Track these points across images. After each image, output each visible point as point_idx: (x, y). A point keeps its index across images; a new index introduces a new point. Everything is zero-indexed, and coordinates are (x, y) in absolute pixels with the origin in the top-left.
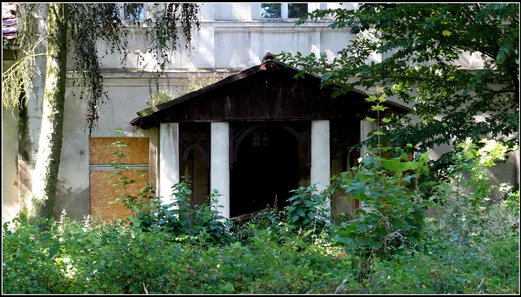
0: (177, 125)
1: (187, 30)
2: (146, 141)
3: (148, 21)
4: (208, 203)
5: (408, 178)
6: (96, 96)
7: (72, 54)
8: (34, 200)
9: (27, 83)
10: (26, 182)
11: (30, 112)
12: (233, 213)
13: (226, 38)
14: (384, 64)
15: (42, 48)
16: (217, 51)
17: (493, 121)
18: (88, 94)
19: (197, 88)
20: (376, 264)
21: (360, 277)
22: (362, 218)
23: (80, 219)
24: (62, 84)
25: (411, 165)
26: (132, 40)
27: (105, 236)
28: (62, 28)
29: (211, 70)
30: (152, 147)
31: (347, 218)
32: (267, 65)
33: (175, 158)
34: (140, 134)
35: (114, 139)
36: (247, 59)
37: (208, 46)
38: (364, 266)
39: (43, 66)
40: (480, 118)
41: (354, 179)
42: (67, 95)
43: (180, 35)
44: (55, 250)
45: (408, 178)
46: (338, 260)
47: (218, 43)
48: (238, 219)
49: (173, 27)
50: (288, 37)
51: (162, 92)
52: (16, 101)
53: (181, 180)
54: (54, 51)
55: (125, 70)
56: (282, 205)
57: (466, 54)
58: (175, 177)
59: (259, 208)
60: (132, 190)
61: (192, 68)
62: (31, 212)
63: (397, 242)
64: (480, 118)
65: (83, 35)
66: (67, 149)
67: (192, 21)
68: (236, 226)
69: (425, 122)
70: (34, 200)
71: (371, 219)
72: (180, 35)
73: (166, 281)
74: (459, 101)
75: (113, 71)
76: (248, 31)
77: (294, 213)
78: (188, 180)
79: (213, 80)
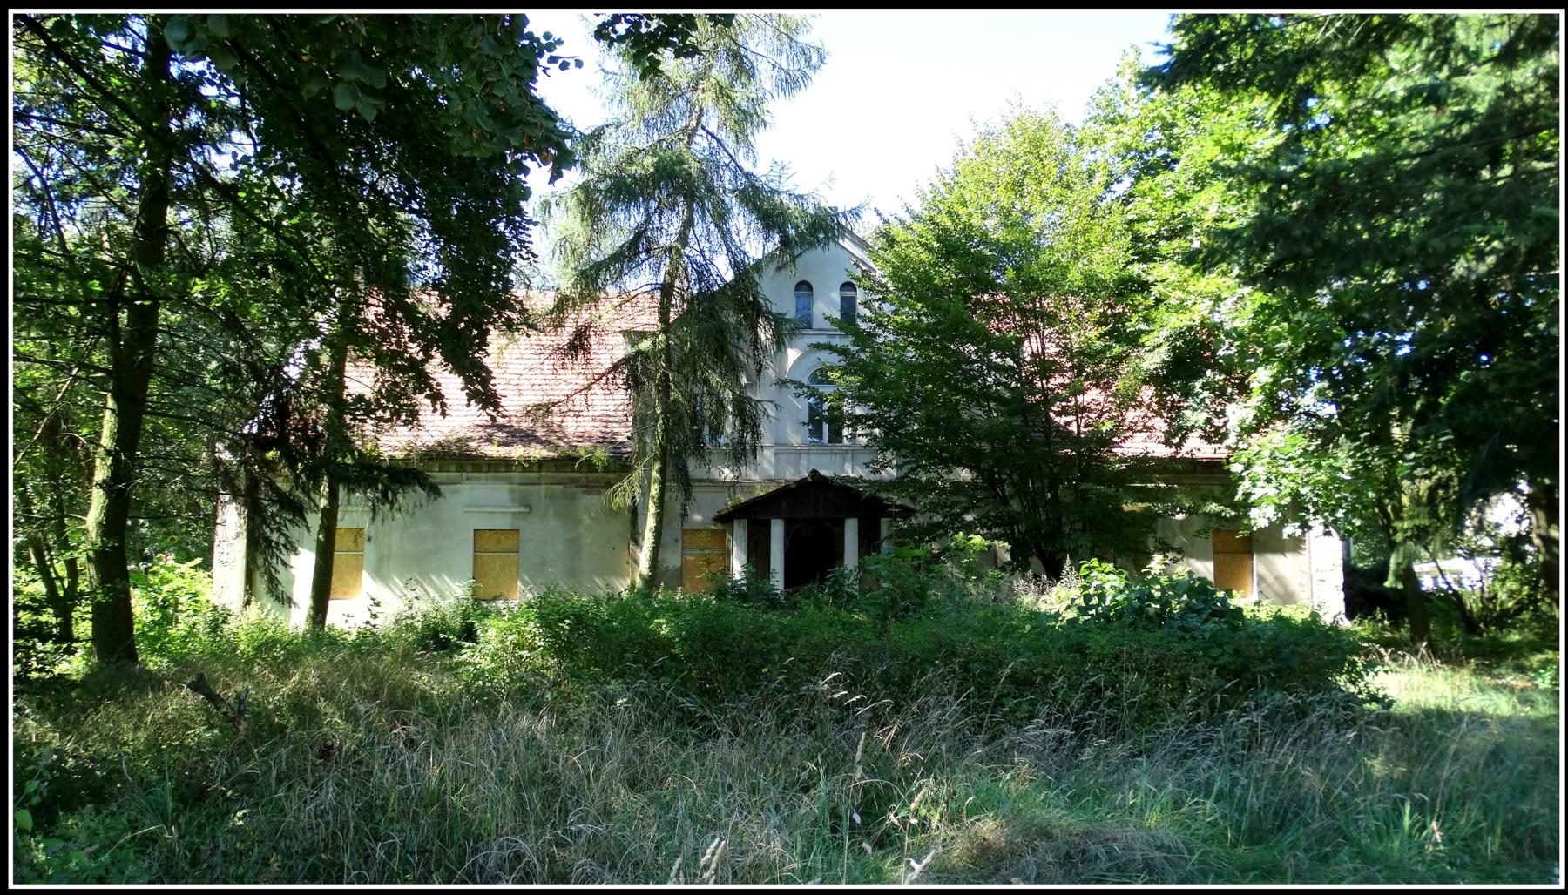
0: (746, 521)
1: (754, 452)
2: (724, 532)
3: (727, 445)
4: (769, 579)
5: (916, 563)
6: (687, 499)
7: (670, 470)
8: (641, 575)
9: (637, 489)
10: (636, 562)
11: (640, 511)
12: (786, 586)
13: (783, 457)
14: (900, 479)
15: (649, 465)
16: (776, 466)
17: (980, 520)
18: (681, 498)
19: (761, 494)
20: (893, 627)
21: (880, 636)
22: (881, 591)
23: (675, 590)
24: (662, 491)
25: (917, 552)
26: (714, 458)
27: (692, 602)
28: (663, 449)
29: (772, 481)
30: (728, 536)
31: (870, 590)
32: (812, 477)
33: (744, 544)
34: (719, 527)
35: (700, 531)
36: (799, 473)
37: (769, 462)
38: (883, 627)
39: (649, 477)
40: (969, 518)
41: (1318, 466)
42: (666, 498)
43: (749, 455)
44: (655, 613)
45: (916, 563)
46: (862, 622)
47: (777, 461)
48: (790, 590)
49: (744, 449)
50: (828, 457)
51: (738, 496)
52: (629, 502)
53: (749, 561)
54: (657, 466)
55: (709, 480)
56: (822, 580)
57: (958, 470)
58: (744, 558)
59: (806, 583)
60: (713, 568)
61: (756, 478)
62: (639, 583)
63: (906, 609)
64: (969, 518)
65: (678, 455)
66: (665, 537)
67: (758, 445)
68: (788, 595)
69: (1156, 563)
70: (641, 575)
71: (888, 592)
72: (749, 455)
73: (734, 639)
74: (954, 504)
75: (700, 481)
76: (799, 453)
77: (830, 587)
78: (1167, 515)
79: (773, 488)
